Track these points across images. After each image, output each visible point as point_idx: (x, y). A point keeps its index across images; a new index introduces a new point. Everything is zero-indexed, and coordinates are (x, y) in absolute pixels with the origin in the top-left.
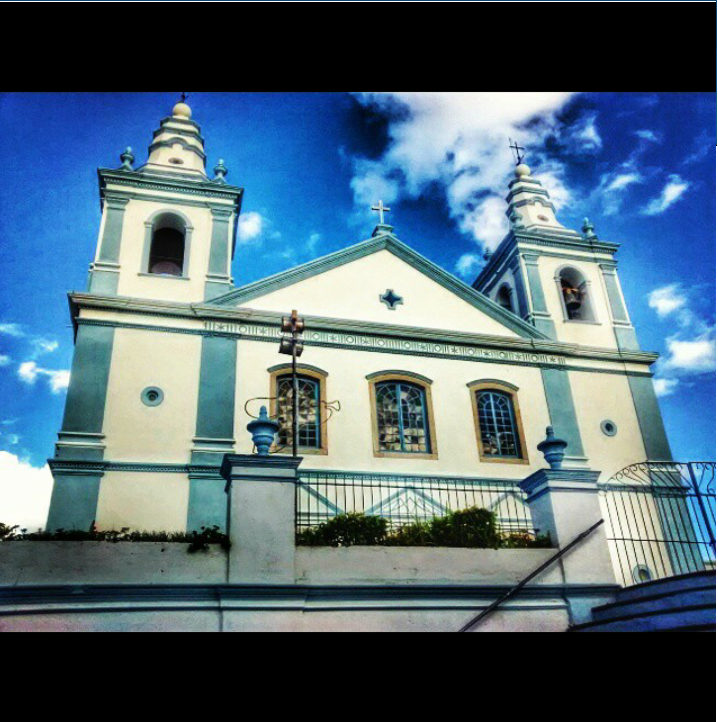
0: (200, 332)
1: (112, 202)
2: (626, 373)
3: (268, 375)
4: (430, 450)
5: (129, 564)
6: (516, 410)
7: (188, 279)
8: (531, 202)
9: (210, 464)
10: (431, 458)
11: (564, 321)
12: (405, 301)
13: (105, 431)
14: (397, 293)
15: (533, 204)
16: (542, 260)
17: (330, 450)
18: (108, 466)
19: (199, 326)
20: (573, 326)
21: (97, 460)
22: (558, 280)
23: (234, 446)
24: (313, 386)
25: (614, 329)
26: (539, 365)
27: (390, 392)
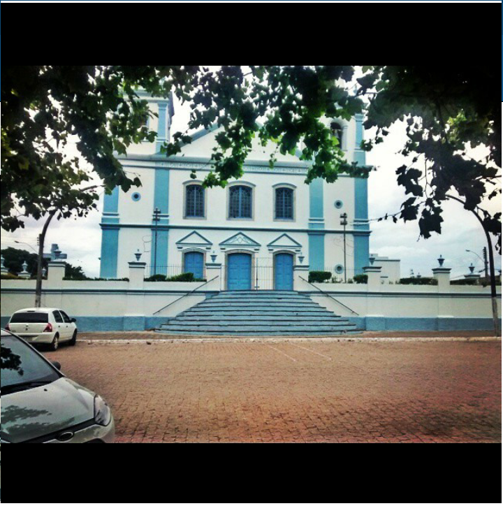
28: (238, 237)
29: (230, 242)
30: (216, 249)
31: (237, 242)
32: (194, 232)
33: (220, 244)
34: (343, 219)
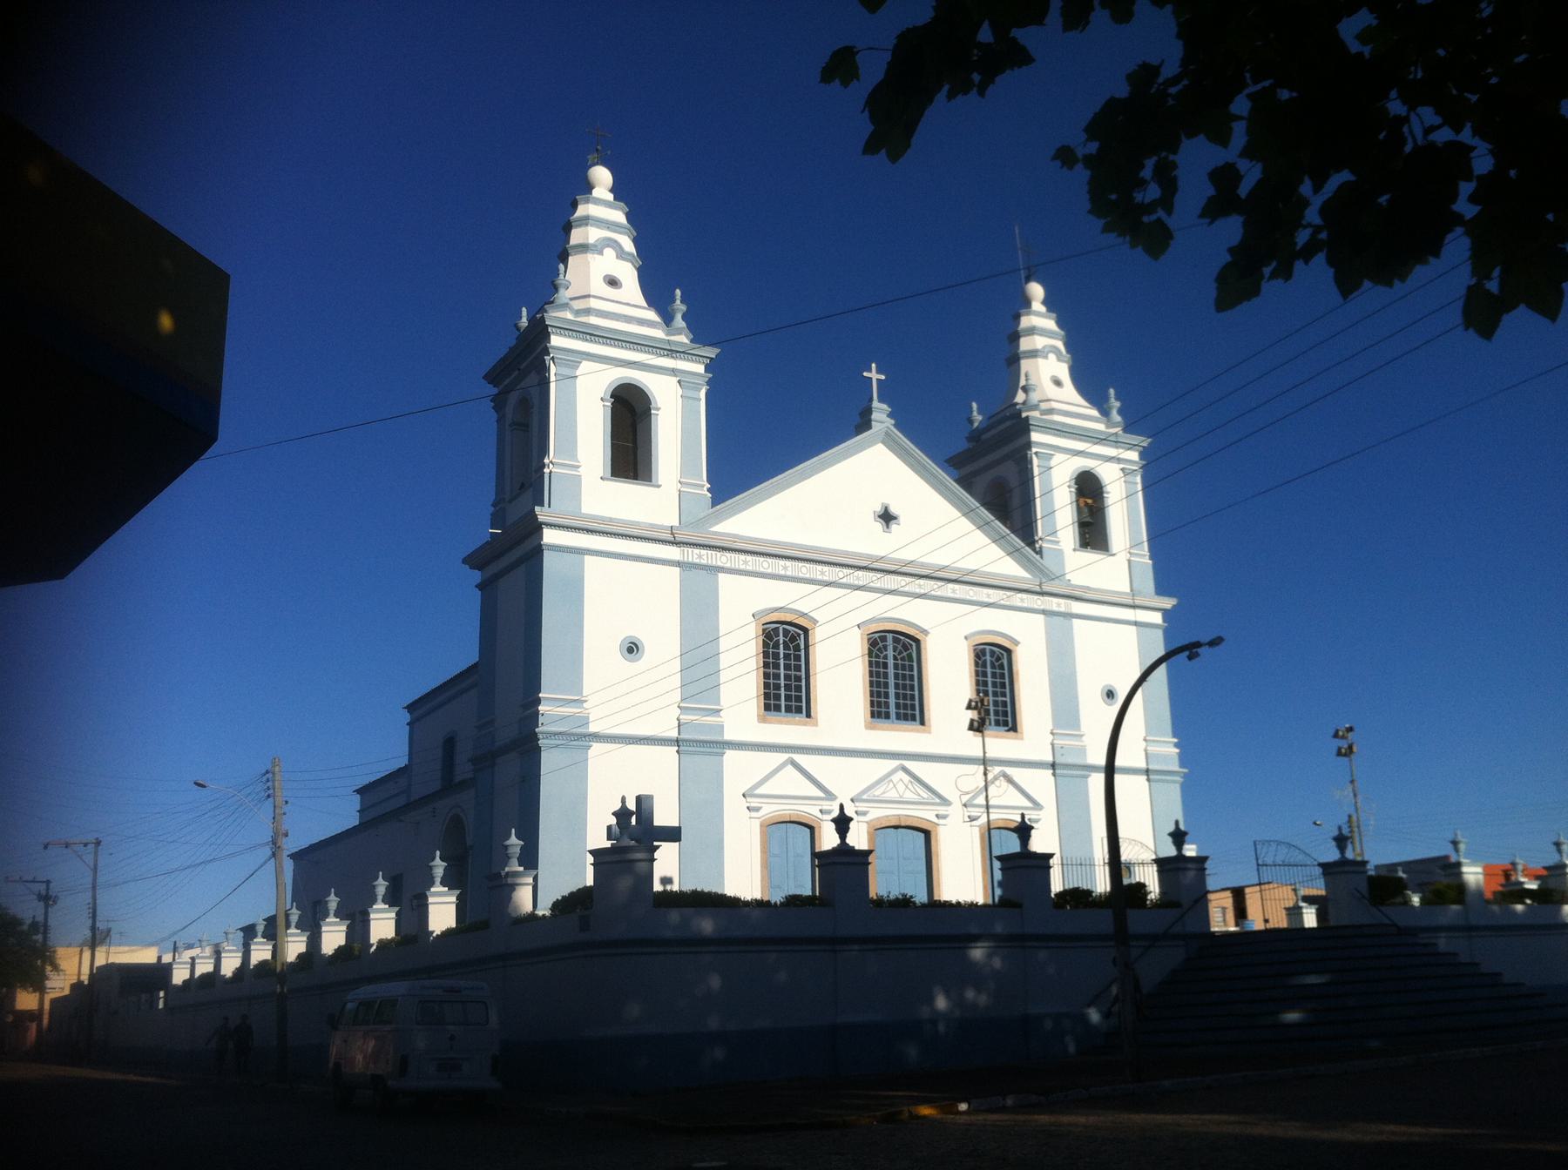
0: (678, 564)
1: (688, 388)
2: (1136, 623)
3: (965, 643)
4: (808, 715)
5: (111, 854)
6: (1014, 671)
7: (659, 486)
8: (597, 249)
9: (702, 738)
10: (924, 731)
11: (1075, 550)
12: (901, 519)
13: (1084, 729)
14: (893, 510)
15: (1046, 357)
16: (1058, 458)
17: (934, 728)
18: (597, 737)
19: (673, 553)
20: (1089, 556)
21: (719, 739)
22: (1073, 490)
23: (1084, 738)
24: (799, 635)
25: (1129, 561)
26: (1044, 612)
27: (900, 647)
28: (895, 778)
29: (878, 792)
30: (956, 812)
31: (892, 795)
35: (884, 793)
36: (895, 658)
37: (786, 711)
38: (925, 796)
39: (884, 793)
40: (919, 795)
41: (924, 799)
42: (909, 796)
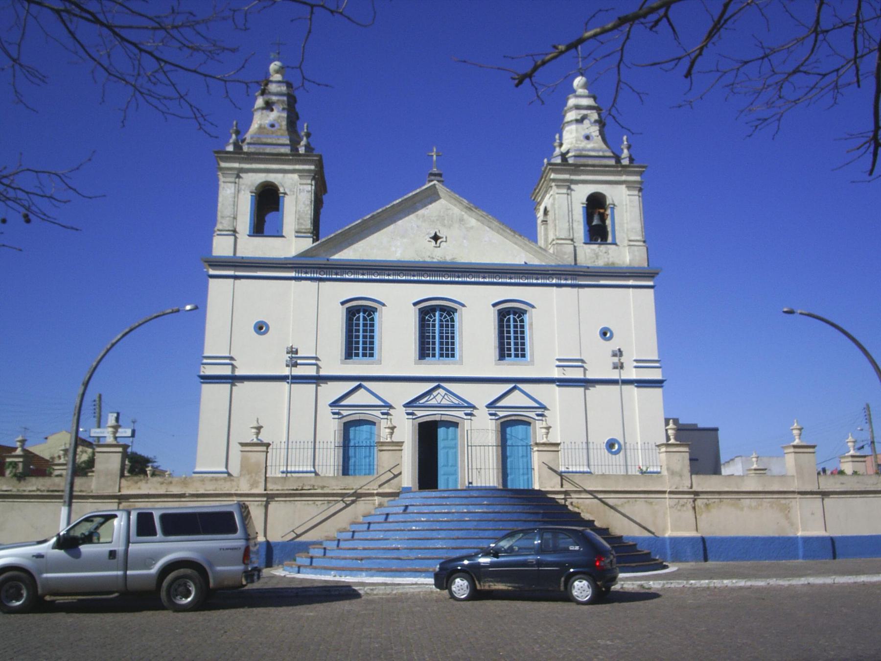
31: (433, 402)
32: (514, 388)
33: (407, 405)
34: (616, 359)
35: (427, 401)
36: (441, 321)
37: (363, 356)
38: (457, 402)
39: (427, 401)
40: (452, 402)
41: (455, 404)
42: (444, 402)
